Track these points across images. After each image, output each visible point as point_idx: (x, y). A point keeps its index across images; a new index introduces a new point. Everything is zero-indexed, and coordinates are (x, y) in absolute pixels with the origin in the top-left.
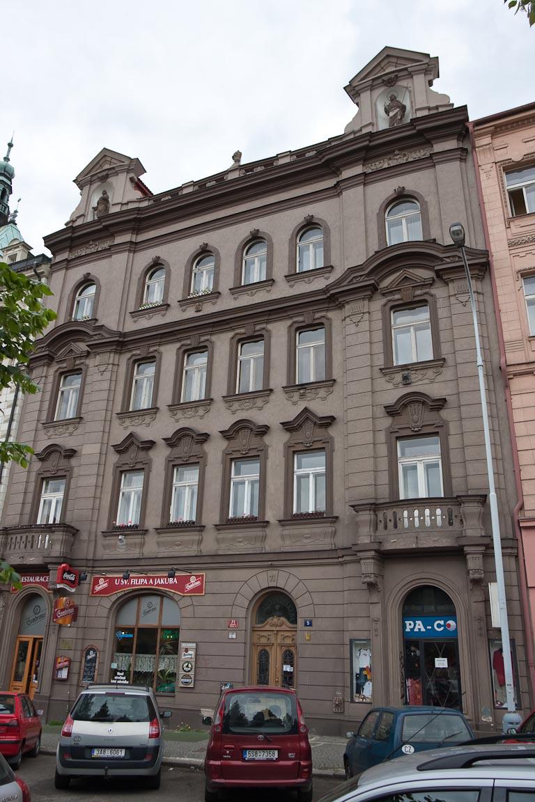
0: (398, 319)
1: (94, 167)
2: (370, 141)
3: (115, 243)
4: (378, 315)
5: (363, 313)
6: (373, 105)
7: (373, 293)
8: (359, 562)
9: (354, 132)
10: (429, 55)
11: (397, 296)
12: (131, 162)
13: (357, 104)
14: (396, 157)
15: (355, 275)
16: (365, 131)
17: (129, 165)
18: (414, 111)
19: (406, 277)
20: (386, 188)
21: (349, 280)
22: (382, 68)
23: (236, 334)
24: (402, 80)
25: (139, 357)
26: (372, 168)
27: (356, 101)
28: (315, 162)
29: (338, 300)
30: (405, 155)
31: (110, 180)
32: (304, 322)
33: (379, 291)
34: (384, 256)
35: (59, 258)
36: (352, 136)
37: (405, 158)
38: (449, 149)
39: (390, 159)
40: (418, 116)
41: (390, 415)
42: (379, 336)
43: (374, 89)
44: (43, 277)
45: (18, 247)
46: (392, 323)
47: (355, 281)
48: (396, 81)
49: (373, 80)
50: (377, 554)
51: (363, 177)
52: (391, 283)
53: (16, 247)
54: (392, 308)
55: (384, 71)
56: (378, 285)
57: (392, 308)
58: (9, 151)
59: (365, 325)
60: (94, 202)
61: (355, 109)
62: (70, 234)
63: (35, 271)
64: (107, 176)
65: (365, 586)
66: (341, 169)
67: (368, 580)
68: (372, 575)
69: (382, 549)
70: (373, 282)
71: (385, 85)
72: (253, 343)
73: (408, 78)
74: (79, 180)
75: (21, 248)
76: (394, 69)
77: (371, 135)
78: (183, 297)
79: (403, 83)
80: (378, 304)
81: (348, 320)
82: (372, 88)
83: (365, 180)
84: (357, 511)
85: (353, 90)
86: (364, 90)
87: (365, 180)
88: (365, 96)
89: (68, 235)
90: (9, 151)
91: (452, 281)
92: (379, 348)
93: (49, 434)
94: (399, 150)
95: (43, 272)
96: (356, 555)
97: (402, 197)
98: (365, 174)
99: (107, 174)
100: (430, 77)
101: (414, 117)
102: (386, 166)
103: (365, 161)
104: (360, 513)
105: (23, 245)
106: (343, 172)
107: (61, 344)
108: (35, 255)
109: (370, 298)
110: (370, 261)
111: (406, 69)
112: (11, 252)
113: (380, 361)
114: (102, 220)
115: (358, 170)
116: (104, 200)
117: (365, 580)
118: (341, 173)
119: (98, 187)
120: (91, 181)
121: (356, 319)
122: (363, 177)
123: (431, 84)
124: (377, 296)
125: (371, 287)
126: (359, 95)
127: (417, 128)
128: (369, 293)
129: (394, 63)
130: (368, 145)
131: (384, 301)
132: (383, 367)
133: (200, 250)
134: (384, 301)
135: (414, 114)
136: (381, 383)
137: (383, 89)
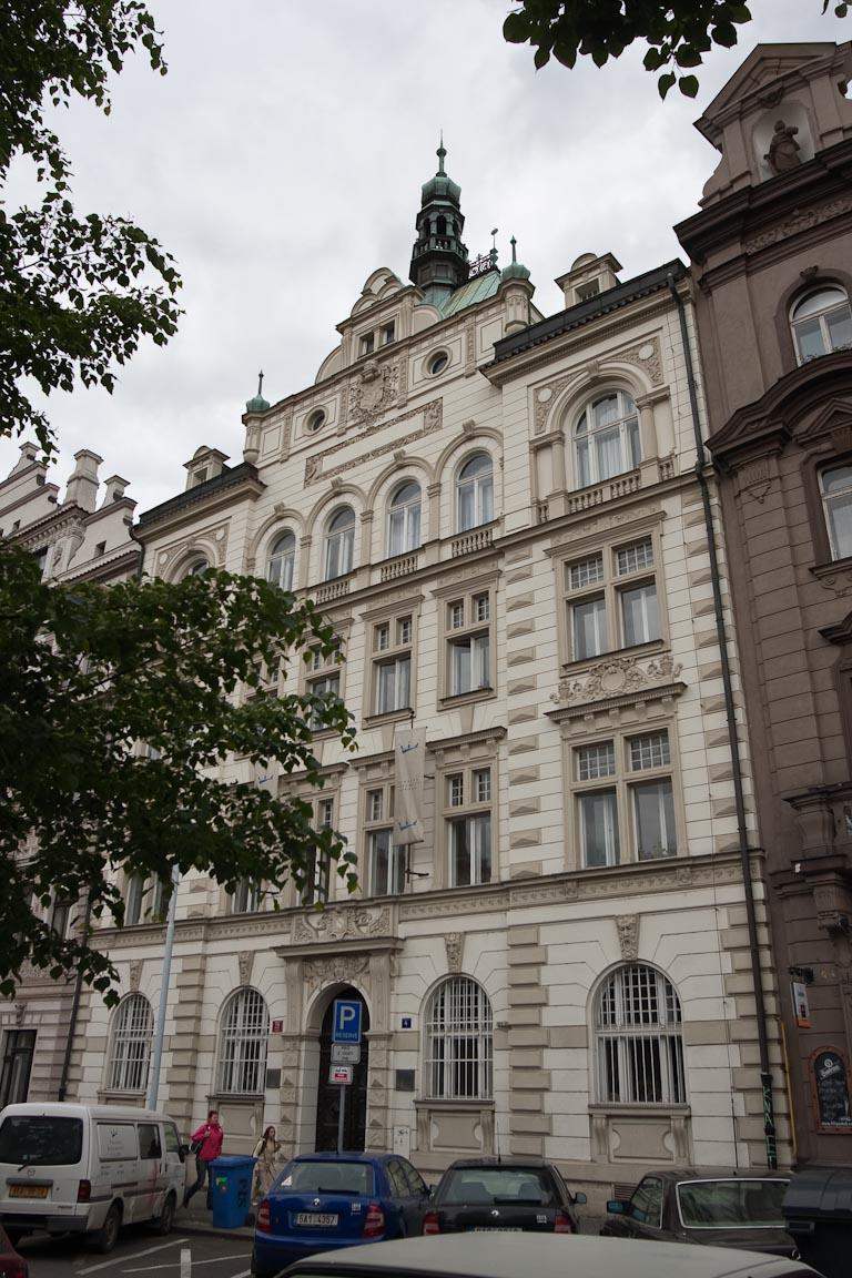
0: (832, 484)
1: (741, 85)
2: (750, 203)
3: (711, 268)
4: (794, 480)
5: (770, 480)
6: (748, 143)
7: (784, 445)
8: (811, 894)
9: (721, 192)
10: (835, 43)
11: (826, 446)
12: (836, 53)
13: (719, 147)
14: (796, 221)
15: (749, 420)
16: (737, 188)
17: (834, 58)
18: (818, 137)
19: (837, 412)
20: (788, 272)
21: (738, 431)
22: (755, 80)
23: (812, 455)
24: (790, 92)
25: (833, 454)
26: (757, 245)
27: (717, 142)
28: (816, 171)
29: (727, 464)
30: (811, 215)
31: (787, 99)
32: (833, 449)
33: (794, 440)
34: (791, 385)
35: (714, 262)
36: (717, 199)
37: (812, 219)
38: (719, 264)
39: (786, 225)
40: (826, 147)
41: (836, 644)
42: (801, 514)
43: (744, 117)
44: (687, 302)
45: (208, 458)
46: (822, 491)
47: (749, 430)
48: (782, 96)
49: (743, 101)
50: (839, 878)
51: (744, 262)
52: (812, 426)
53: (205, 458)
54: (819, 465)
55: (759, 84)
56: (791, 431)
57: (819, 465)
58: (442, 163)
59: (774, 500)
60: (762, 147)
61: (717, 156)
62: (745, 205)
63: (674, 291)
64: (782, 92)
65: (825, 934)
66: (706, 255)
67: (828, 922)
68: (836, 914)
69: (848, 867)
70: (780, 426)
71: (764, 106)
72: (846, 468)
73: (802, 87)
74: (710, 118)
75: (212, 459)
76: (773, 77)
77: (750, 191)
78: (785, 369)
79: (799, 96)
80: (794, 461)
81: (745, 496)
82: (741, 115)
83: (747, 267)
84: (798, 808)
85: (340, 328)
86: (729, 121)
87: (747, 267)
88: (732, 132)
89: (739, 208)
90: (442, 163)
91: (742, 467)
92: (804, 533)
93: (836, 587)
94: (799, 209)
95: (687, 293)
96: (804, 881)
97: (814, 284)
98: (746, 257)
99: (782, 89)
100: (841, 78)
101: (821, 149)
102: (780, 237)
103: (744, 236)
104: (804, 810)
105: (214, 455)
106: (709, 260)
107: (816, 397)
108: (231, 467)
109: (779, 455)
110: (770, 394)
111: (797, 73)
112: (198, 466)
113: (808, 555)
114: (824, 160)
115: (735, 251)
116: (786, 135)
117: (825, 922)
118: (706, 261)
119: (760, 120)
120: (741, 113)
121: (759, 492)
122: (744, 262)
123: (843, 90)
124: (790, 450)
125: (778, 436)
126: (722, 131)
127: (829, 165)
128: (776, 445)
129: (774, 67)
130: (748, 208)
131: (803, 455)
132: (814, 565)
133: (803, 281)
134: (803, 455)
135: (820, 145)
136: (814, 590)
137: (760, 113)
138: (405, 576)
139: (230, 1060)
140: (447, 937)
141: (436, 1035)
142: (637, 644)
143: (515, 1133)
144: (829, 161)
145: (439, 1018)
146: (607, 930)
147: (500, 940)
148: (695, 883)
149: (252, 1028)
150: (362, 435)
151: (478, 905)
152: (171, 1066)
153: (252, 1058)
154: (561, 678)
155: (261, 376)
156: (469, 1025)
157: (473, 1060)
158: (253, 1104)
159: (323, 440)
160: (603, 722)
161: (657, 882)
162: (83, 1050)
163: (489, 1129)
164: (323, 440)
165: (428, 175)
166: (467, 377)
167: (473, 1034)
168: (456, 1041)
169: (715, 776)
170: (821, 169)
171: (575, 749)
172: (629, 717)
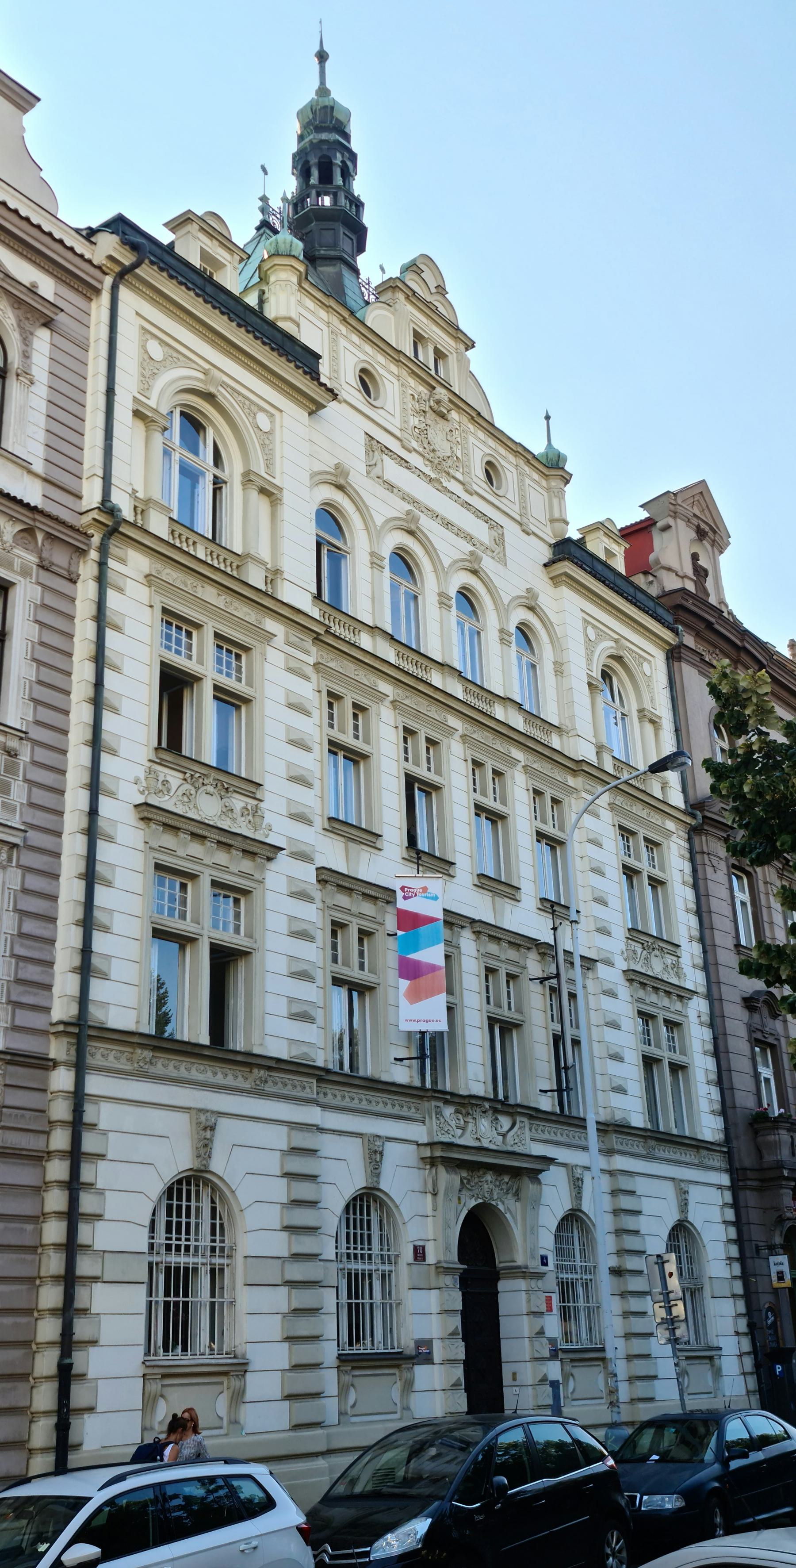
28: (736, 637)
114: (746, 637)
138: (416, 678)
139: (181, 1299)
140: (208, 1114)
141: (383, 1268)
142: (203, 761)
143: (317, 1395)
144: (748, 642)
145: (183, 1236)
146: (180, 1124)
147: (279, 1138)
148: (152, 1070)
149: (174, 1242)
150: (422, 474)
151: (171, 1067)
152: (734, 1314)
153: (177, 1294)
154: (150, 761)
155: (548, 418)
156: (356, 1255)
157: (360, 1301)
158: (398, 1366)
159: (8, 185)
160: (196, 849)
161: (230, 1077)
162: (95, 1279)
163: (718, 1373)
164: (8, 185)
165: (307, 94)
166: (524, 531)
167: (191, 1260)
168: (349, 1274)
169: (293, 970)
170: (767, 660)
171: (158, 867)
172: (222, 857)
